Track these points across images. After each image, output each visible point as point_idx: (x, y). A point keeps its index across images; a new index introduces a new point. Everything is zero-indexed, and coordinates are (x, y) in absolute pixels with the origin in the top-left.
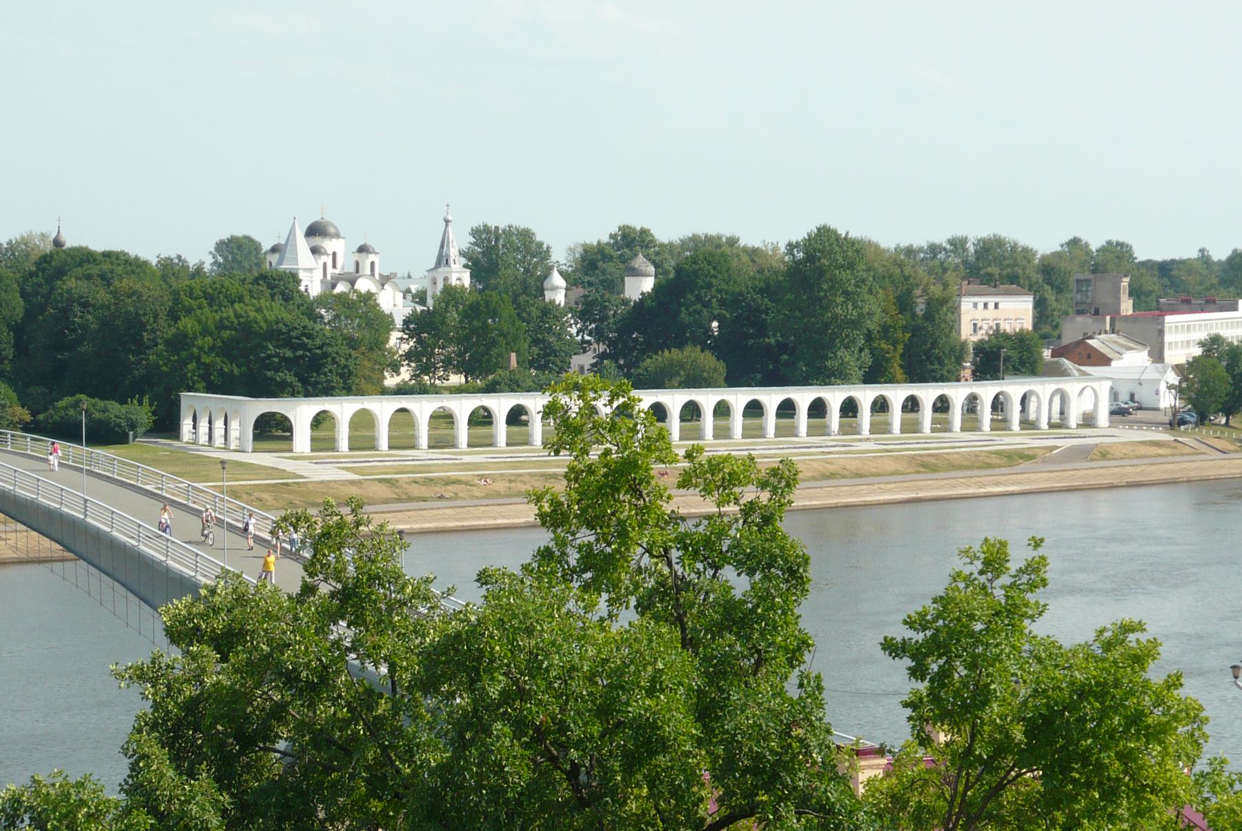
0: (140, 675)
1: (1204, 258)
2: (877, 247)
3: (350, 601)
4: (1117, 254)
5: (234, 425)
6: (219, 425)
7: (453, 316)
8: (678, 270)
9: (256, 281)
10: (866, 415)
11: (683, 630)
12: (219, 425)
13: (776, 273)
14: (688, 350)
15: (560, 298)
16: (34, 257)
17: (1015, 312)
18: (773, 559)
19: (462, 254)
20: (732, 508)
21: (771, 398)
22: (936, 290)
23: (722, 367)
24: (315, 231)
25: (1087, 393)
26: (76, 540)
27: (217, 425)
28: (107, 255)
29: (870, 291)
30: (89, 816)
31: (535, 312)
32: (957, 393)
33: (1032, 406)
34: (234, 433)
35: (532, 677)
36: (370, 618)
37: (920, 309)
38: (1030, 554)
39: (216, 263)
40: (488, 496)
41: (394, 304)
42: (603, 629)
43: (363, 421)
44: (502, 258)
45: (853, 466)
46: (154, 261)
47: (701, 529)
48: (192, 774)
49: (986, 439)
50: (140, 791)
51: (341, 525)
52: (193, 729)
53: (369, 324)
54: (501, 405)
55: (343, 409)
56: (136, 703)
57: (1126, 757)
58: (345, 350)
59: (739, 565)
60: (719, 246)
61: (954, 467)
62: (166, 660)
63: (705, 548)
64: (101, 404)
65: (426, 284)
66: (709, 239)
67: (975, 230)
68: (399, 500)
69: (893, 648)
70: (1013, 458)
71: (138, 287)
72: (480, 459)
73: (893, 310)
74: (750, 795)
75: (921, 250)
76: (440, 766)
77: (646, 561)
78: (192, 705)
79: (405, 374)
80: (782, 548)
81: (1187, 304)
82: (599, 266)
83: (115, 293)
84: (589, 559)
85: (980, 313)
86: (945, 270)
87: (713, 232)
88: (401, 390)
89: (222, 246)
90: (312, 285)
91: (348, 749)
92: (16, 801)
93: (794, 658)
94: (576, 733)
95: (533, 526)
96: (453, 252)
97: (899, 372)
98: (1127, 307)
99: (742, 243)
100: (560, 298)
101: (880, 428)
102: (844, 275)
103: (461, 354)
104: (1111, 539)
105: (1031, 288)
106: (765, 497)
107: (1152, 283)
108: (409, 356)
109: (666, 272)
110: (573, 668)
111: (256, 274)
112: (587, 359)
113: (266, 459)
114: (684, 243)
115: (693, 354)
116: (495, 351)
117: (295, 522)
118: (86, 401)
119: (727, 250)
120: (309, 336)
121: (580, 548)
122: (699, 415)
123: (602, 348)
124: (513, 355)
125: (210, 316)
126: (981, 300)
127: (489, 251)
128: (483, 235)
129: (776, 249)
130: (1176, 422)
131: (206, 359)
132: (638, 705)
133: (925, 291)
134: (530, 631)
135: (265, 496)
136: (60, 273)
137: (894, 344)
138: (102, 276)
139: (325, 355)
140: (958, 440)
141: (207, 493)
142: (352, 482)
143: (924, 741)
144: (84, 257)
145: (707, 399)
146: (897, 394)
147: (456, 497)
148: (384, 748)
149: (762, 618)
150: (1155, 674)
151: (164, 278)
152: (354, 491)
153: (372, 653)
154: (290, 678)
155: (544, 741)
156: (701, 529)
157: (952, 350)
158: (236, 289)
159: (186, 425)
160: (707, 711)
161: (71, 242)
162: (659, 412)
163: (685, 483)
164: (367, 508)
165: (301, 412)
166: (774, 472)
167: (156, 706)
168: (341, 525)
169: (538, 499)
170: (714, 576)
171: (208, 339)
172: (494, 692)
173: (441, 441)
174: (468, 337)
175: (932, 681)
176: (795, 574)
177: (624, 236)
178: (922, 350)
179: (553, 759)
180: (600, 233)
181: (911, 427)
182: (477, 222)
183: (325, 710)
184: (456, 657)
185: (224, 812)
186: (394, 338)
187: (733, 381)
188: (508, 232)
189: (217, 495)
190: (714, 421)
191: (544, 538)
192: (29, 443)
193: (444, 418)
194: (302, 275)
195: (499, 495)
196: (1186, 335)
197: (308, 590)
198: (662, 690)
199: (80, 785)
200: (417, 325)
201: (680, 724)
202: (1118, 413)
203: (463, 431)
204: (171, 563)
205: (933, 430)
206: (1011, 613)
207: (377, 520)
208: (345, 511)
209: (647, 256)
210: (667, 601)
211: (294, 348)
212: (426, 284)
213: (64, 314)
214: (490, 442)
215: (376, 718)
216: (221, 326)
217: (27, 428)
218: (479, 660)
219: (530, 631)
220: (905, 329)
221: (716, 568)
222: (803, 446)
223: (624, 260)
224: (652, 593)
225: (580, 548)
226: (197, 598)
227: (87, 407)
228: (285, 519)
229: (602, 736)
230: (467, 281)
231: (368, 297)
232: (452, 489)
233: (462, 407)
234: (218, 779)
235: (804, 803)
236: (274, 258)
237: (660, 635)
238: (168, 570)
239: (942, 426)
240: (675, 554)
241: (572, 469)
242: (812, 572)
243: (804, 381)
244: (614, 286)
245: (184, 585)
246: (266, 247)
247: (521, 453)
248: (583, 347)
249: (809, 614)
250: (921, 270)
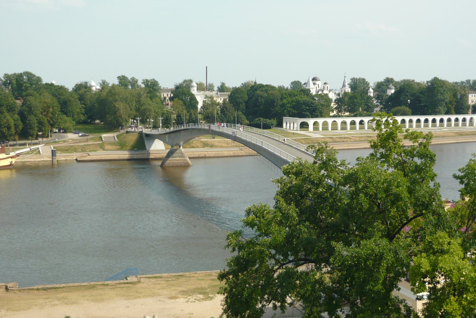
0: (278, 181)
2: (448, 82)
3: (325, 165)
5: (295, 124)
6: (292, 124)
7: (347, 99)
8: (400, 88)
9: (300, 91)
10: (445, 122)
11: (405, 172)
12: (292, 124)
13: (424, 88)
14: (402, 107)
15: (372, 95)
16: (250, 86)
18: (427, 155)
19: (348, 84)
20: (416, 144)
21: (422, 118)
22: (463, 92)
23: (410, 110)
24: (314, 79)
27: (291, 124)
28: (267, 85)
29: (447, 93)
30: (267, 213)
31: (366, 98)
34: (295, 127)
35: (369, 183)
36: (329, 169)
37: (459, 97)
39: (291, 87)
40: (354, 141)
41: (332, 96)
42: (385, 172)
43: (325, 124)
44: (358, 85)
45: (442, 134)
46: (277, 87)
47: (409, 149)
48: (290, 204)
51: (322, 148)
52: (288, 194)
53: (327, 101)
54: (357, 120)
55: (321, 121)
56: (276, 188)
58: (321, 107)
59: (419, 157)
60: (410, 82)
61: (467, 135)
62: (284, 178)
63: (411, 153)
64: (265, 120)
65: (340, 91)
66: (408, 80)
68: (334, 142)
69: (456, 177)
71: (273, 93)
72: (353, 132)
73: (452, 97)
75: (459, 83)
76: (347, 203)
77: (396, 156)
78: (290, 188)
79: (335, 113)
80: (430, 152)
82: (381, 87)
83: (268, 94)
85: (473, 98)
86: (465, 88)
87: (408, 79)
88: (334, 116)
89: (292, 83)
90: (313, 92)
91: (326, 199)
92: (250, 209)
93: (432, 179)
94: (379, 196)
95: (368, 148)
96: (346, 84)
97: (453, 112)
99: (415, 81)
100: (372, 95)
101: (449, 125)
102: (440, 89)
103: (348, 108)
106: (425, 141)
108: (336, 108)
109: (397, 88)
110: (379, 181)
111: (300, 89)
112: (378, 109)
113: (302, 132)
114: (402, 81)
116: (356, 107)
117: (312, 147)
118: (262, 119)
119: (412, 83)
120: (313, 104)
121: (380, 153)
123: (382, 106)
124: (360, 108)
125: (290, 99)
127: (355, 84)
128: (353, 79)
129: (424, 83)
131: (289, 109)
132: (395, 190)
133: (460, 93)
135: (302, 141)
136: (256, 90)
137: (452, 105)
138: (265, 90)
139: (317, 108)
141: (288, 140)
142: (323, 138)
143: (463, 199)
144: (261, 86)
145: (407, 118)
146: (453, 117)
147: (347, 141)
148: (334, 199)
149: (424, 169)
151: (279, 91)
152: (323, 140)
153: (329, 177)
154: (312, 183)
155: (372, 198)
156: (409, 149)
157: (467, 106)
158: (296, 93)
159: (284, 124)
160: (411, 191)
161: (258, 82)
163: (406, 137)
164: (328, 144)
165: (311, 122)
166: (427, 135)
167: (281, 189)
168: (322, 148)
169: (371, 142)
170: (412, 160)
171: (289, 105)
172: (360, 187)
173: (344, 128)
174: (350, 104)
175: (465, 185)
176: (432, 159)
177: (387, 80)
178: (459, 107)
179: (374, 202)
181: (457, 125)
182: (352, 77)
184: (351, 178)
185: (297, 213)
186: (332, 104)
187: (414, 114)
188: (359, 79)
189: (293, 141)
190: (411, 122)
191: (372, 151)
193: (344, 123)
194: (311, 90)
195: (357, 141)
197: (315, 163)
198: (400, 186)
199: (265, 206)
200: (338, 101)
201: (405, 195)
203: (348, 126)
204: (281, 156)
205: (462, 126)
207: (331, 146)
208: (323, 144)
209: (392, 84)
210: (401, 165)
211: (309, 107)
212: (340, 91)
213: (257, 99)
214: (355, 128)
215: (332, 192)
216: (292, 101)
217: (248, 125)
218: (357, 179)
220: (455, 102)
221: (413, 158)
222: (436, 130)
223: (387, 85)
224: (398, 164)
225: (380, 153)
226: (290, 165)
227: (262, 120)
228: (309, 146)
229: (386, 197)
230: (350, 91)
231: (326, 95)
232: (349, 140)
233: (348, 120)
234: (296, 205)
235: (434, 213)
236: (305, 86)
237: (398, 173)
238: (281, 158)
239: (464, 125)
240: (403, 154)
241: (378, 135)
242: (436, 158)
243: (430, 114)
244: (385, 92)
245: (285, 162)
246: (303, 83)
247: (362, 131)
248: (377, 106)
249: (436, 169)
250: (459, 88)
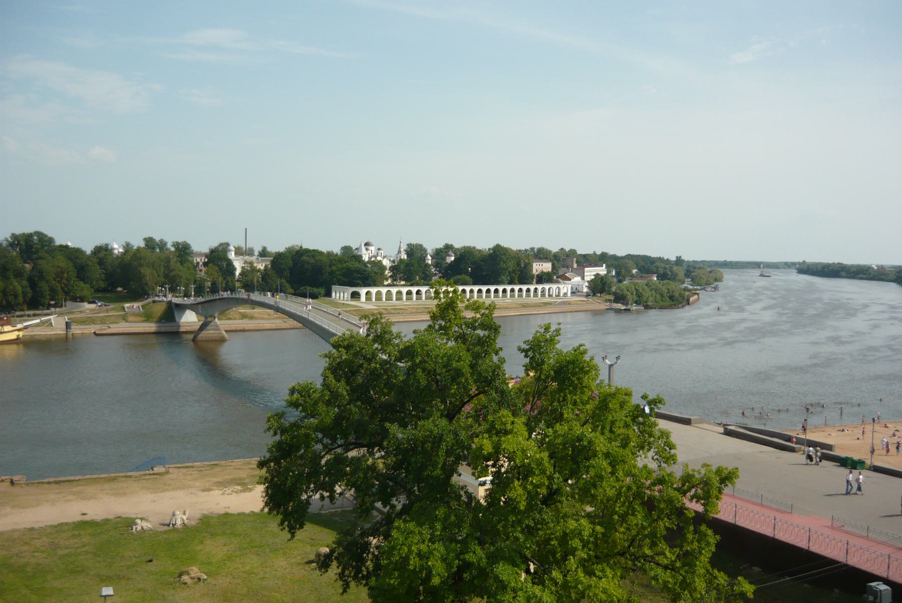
0: (326, 356)
1: (595, 254)
3: (379, 338)
4: (573, 252)
7: (402, 267)
15: (430, 262)
17: (547, 267)
22: (527, 261)
24: (367, 244)
25: (565, 288)
26: (306, 323)
27: (341, 294)
32: (532, 288)
37: (523, 265)
38: (557, 327)
41: (386, 263)
43: (379, 294)
48: (339, 381)
49: (539, 299)
50: (325, 385)
52: (336, 369)
54: (414, 289)
55: (373, 290)
56: (324, 363)
57: (579, 379)
63: (472, 325)
67: (537, 246)
70: (546, 304)
74: (483, 388)
77: (457, 329)
78: (339, 364)
79: (389, 281)
81: (590, 266)
82: (440, 254)
84: (441, 328)
88: (389, 285)
91: (379, 376)
92: (294, 388)
93: (497, 353)
94: (438, 371)
98: (575, 266)
100: (430, 262)
101: (512, 296)
105: (551, 261)
107: (582, 260)
108: (391, 277)
115: (464, 276)
118: (308, 288)
125: (340, 266)
127: (412, 250)
128: (409, 245)
130: (587, 295)
134: (427, 345)
140: (532, 299)
146: (517, 288)
150: (587, 358)
154: (365, 358)
155: (429, 373)
159: (333, 294)
160: (472, 366)
161: (304, 247)
162: (464, 291)
165: (363, 291)
172: (418, 361)
178: (523, 276)
180: (440, 245)
181: (520, 296)
183: (373, 365)
184: (407, 352)
187: (475, 284)
189: (344, 312)
192: (294, 298)
196: (590, 273)
200: (392, 269)
201: (467, 370)
202: (573, 293)
206: (551, 341)
210: (462, 338)
214: (411, 299)
216: (343, 269)
217: (293, 294)
219: (427, 345)
222: (499, 301)
227: (309, 289)
231: (380, 261)
232: (406, 309)
233: (404, 290)
242: (501, 330)
244: (444, 259)
245: (333, 335)
247: (420, 302)
248: (436, 275)
249: (499, 342)
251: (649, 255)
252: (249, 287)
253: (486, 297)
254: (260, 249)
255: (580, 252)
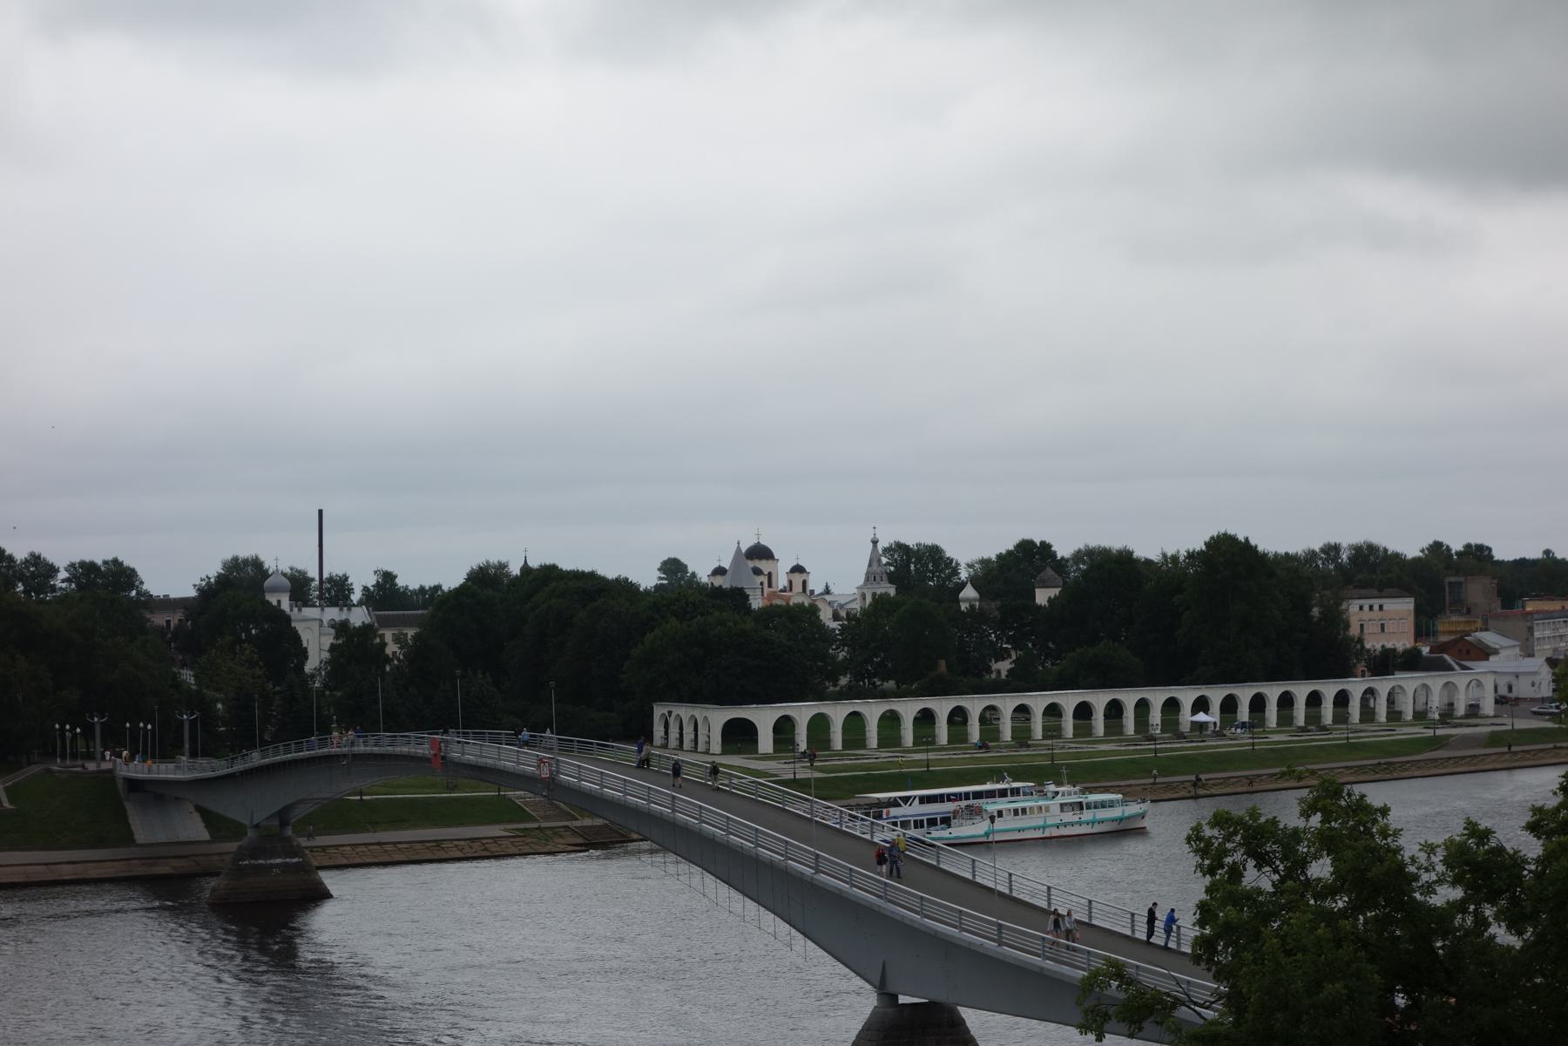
4: (1478, 555)
33: (1400, 699)
43: (819, 725)
67: (1349, 536)
104: (100, 914)
122: (1060, 715)
126: (1366, 603)
159: (658, 731)
161: (534, 563)
165: (764, 718)
202: (1500, 701)
251: (568, 562)
252: (359, 716)
253: (952, 739)
254: (371, 581)
255: (1504, 552)
